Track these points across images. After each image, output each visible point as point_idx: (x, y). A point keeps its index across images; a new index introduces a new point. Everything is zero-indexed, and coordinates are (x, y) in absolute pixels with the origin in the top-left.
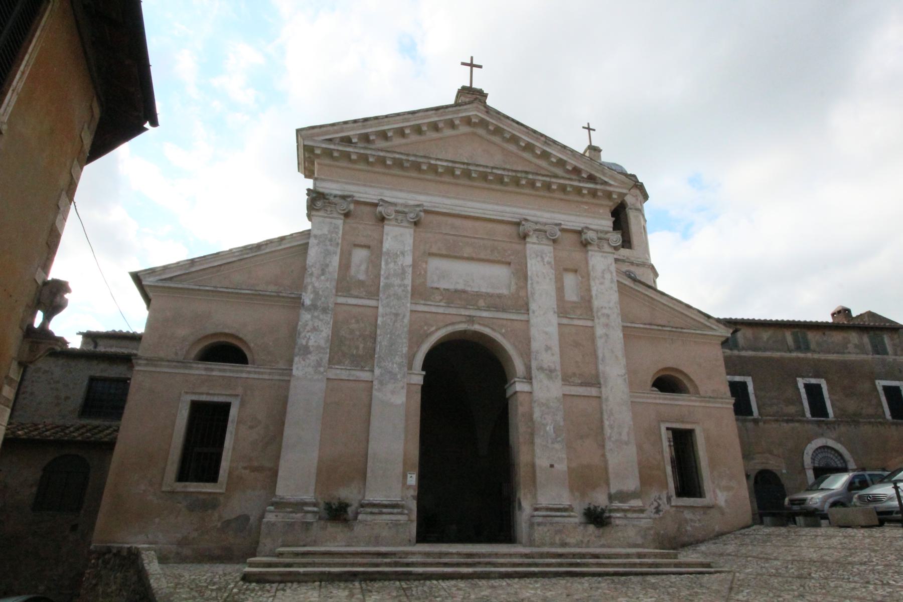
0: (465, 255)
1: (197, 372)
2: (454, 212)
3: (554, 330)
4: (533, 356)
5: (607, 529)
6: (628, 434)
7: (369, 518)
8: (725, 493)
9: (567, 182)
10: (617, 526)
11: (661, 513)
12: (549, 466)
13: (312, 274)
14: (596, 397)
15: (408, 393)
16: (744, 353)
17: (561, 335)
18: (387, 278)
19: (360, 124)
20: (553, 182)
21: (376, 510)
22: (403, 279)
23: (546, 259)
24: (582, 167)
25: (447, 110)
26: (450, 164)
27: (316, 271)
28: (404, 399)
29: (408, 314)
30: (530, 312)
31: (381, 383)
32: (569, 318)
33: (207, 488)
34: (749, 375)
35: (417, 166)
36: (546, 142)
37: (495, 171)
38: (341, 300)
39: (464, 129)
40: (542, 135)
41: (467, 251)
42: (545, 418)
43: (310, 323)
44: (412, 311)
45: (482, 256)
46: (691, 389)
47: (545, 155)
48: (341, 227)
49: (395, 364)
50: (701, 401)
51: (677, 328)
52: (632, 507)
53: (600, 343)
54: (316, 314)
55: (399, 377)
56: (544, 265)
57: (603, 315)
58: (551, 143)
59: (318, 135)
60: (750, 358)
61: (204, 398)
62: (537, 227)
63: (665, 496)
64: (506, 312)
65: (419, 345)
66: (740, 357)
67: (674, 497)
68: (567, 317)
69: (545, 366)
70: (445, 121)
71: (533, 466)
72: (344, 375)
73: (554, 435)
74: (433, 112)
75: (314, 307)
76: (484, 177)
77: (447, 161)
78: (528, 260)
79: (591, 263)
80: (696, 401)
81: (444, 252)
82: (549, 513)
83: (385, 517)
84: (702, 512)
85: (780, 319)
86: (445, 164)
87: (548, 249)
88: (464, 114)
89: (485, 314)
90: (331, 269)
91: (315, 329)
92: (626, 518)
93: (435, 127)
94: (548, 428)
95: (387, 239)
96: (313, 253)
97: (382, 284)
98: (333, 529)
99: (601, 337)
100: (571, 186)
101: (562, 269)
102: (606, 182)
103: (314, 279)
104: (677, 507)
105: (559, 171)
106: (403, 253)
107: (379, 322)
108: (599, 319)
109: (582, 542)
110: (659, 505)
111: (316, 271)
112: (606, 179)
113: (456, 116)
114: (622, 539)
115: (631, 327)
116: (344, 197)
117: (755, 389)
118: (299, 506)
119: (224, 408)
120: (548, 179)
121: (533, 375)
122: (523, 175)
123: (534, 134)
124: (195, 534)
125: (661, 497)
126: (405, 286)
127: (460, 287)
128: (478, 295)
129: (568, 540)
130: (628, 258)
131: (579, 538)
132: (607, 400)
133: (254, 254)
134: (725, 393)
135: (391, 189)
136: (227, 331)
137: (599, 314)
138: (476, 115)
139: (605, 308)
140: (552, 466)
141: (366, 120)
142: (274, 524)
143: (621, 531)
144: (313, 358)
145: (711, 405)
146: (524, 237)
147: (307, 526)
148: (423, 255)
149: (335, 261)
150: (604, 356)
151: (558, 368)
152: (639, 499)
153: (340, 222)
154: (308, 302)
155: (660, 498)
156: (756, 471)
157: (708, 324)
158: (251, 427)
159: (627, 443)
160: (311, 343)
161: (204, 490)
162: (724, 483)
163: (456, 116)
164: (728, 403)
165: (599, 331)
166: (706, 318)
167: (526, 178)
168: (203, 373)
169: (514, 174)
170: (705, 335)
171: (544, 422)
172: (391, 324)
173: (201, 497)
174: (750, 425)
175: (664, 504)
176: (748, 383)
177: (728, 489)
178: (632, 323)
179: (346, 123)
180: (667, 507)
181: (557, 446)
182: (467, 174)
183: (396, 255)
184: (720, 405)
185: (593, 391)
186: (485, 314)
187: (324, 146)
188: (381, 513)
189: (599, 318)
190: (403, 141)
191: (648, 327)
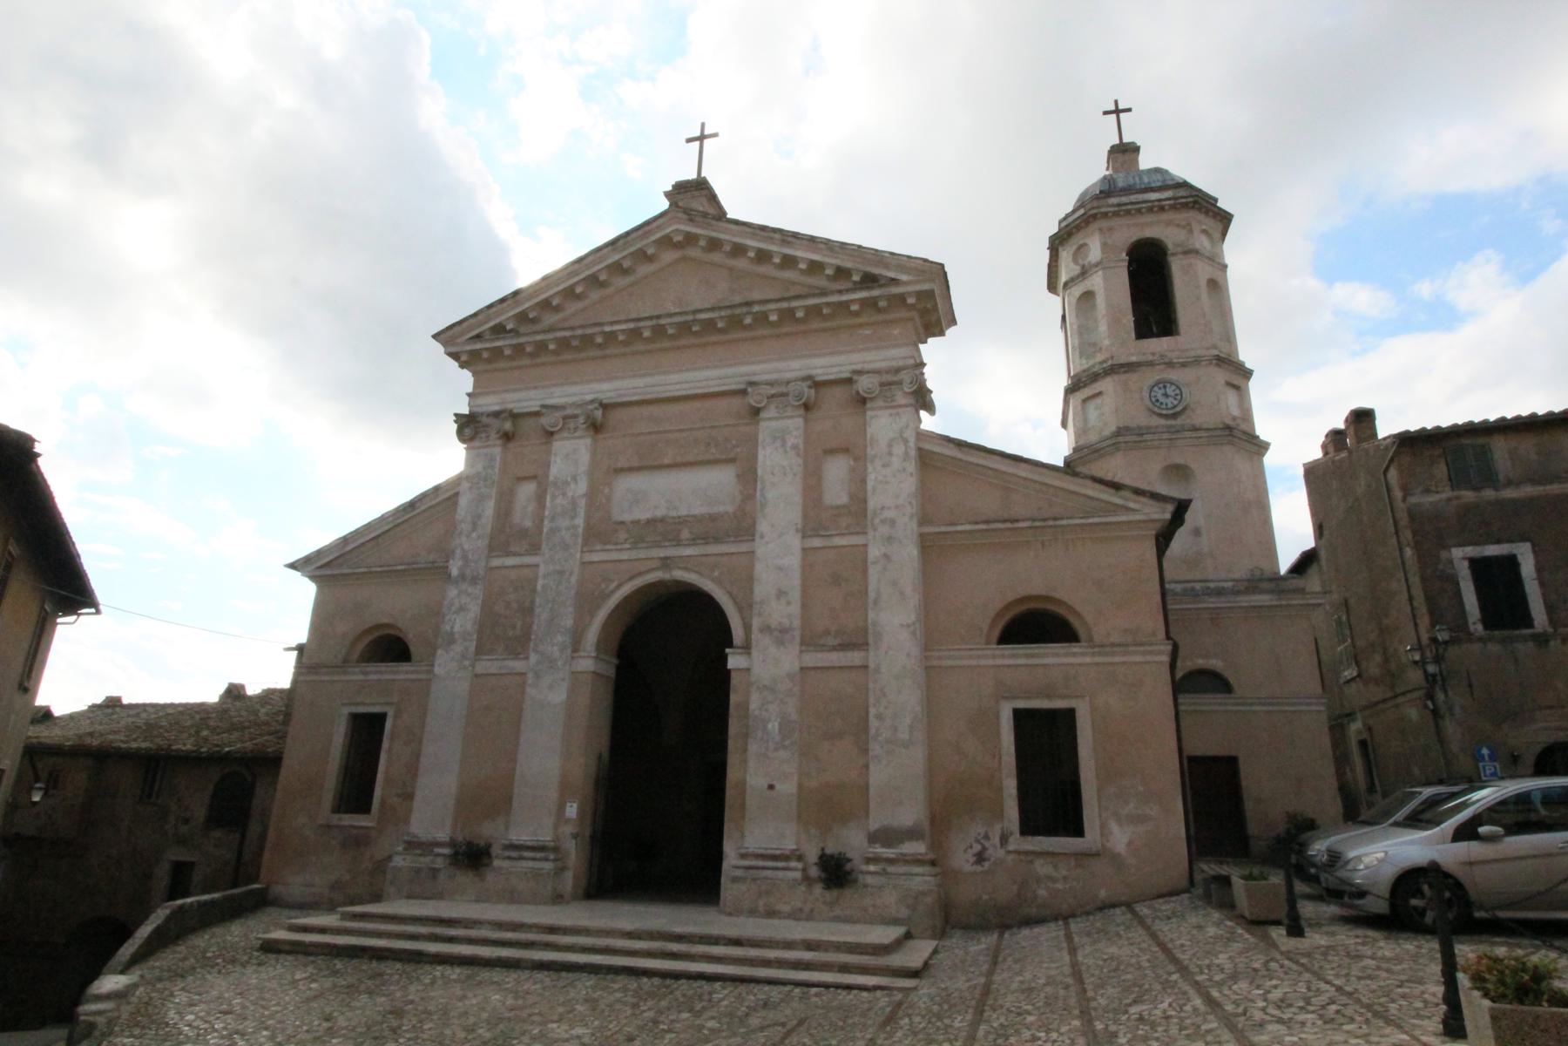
0: (666, 461)
1: (354, 677)
2: (649, 397)
3: (794, 561)
10: (866, 886)
11: (986, 864)
12: (766, 786)
13: (460, 534)
14: (861, 667)
15: (572, 690)
16: (1509, 493)
17: (807, 568)
18: (553, 519)
20: (795, 308)
21: (514, 854)
22: (573, 518)
23: (791, 441)
25: (629, 238)
26: (632, 325)
27: (465, 527)
28: (564, 696)
29: (576, 570)
30: (757, 536)
32: (823, 536)
33: (361, 821)
34: (1523, 539)
35: (587, 341)
36: (783, 241)
38: (496, 562)
39: (669, 256)
40: (775, 230)
42: (767, 710)
45: (691, 458)
47: (789, 262)
49: (555, 645)
50: (1094, 654)
51: (1045, 520)
52: (901, 854)
53: (873, 573)
55: (559, 663)
56: (786, 452)
57: (883, 521)
58: (790, 239)
59: (462, 334)
60: (1529, 503)
64: (723, 542)
65: (592, 614)
66: (1499, 503)
68: (818, 536)
72: (493, 667)
73: (778, 738)
74: (610, 248)
75: (462, 577)
76: (684, 328)
78: (760, 449)
80: (1083, 654)
81: (635, 464)
82: (760, 863)
83: (524, 864)
84: (1073, 863)
85: (1525, 412)
86: (624, 327)
87: (794, 425)
88: (658, 236)
89: (688, 551)
90: (483, 520)
92: (884, 873)
94: (770, 726)
95: (555, 462)
96: (463, 502)
97: (545, 530)
98: (464, 878)
99: (875, 563)
102: (893, 280)
103: (464, 539)
104: (1019, 853)
106: (574, 479)
108: (875, 530)
110: (984, 849)
111: (465, 527)
112: (891, 274)
114: (871, 909)
116: (496, 414)
117: (1539, 569)
118: (426, 847)
120: (785, 305)
121: (754, 643)
122: (744, 310)
123: (762, 233)
124: (348, 877)
125: (990, 834)
126: (575, 527)
127: (659, 513)
128: (682, 521)
132: (877, 670)
133: (408, 516)
134: (1154, 634)
137: (877, 521)
138: (677, 230)
139: (889, 508)
140: (771, 787)
143: (872, 895)
144: (458, 648)
145: (1116, 659)
146: (756, 412)
147: (434, 872)
148: (606, 472)
149: (489, 509)
150: (878, 593)
151: (797, 623)
152: (920, 842)
154: (455, 572)
155: (987, 837)
156: (1538, 749)
160: (457, 628)
161: (356, 824)
164: (1160, 653)
165: (874, 552)
166: (1112, 491)
168: (361, 677)
169: (729, 312)
172: (554, 587)
174: (1525, 649)
175: (995, 846)
176: (1520, 558)
179: (490, 306)
180: (1001, 853)
181: (782, 754)
182: (659, 331)
184: (1138, 658)
185: (855, 657)
186: (688, 551)
187: (468, 348)
188: (521, 858)
190: (579, 305)
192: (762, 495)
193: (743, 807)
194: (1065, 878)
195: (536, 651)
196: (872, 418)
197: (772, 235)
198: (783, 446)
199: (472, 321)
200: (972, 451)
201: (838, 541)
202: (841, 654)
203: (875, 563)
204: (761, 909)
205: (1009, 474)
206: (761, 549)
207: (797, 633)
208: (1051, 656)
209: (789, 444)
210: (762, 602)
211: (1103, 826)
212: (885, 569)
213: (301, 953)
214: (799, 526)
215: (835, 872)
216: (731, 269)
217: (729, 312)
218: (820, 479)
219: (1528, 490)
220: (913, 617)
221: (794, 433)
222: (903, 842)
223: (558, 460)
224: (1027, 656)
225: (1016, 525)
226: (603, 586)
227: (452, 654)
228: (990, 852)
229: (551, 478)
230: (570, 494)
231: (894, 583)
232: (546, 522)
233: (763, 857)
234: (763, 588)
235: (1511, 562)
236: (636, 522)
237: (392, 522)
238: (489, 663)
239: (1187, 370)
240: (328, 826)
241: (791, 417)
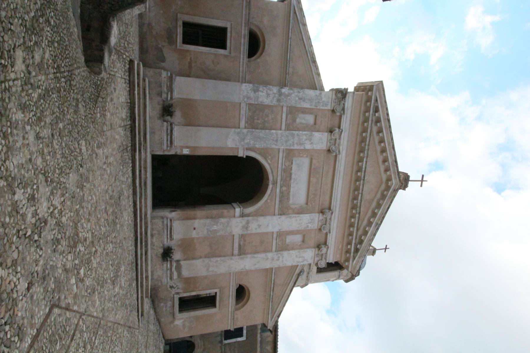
0: (311, 179)
2: (336, 171)
3: (270, 229)
4: (255, 218)
5: (161, 259)
7: (165, 128)
10: (163, 265)
11: (170, 289)
15: (232, 148)
16: (259, 335)
18: (298, 135)
19: (386, 117)
22: (297, 144)
23: (310, 225)
24: (363, 245)
25: (395, 167)
26: (363, 169)
28: (230, 146)
33: (180, 38)
34: (247, 338)
37: (360, 195)
38: (285, 109)
39: (384, 178)
40: (381, 222)
43: (271, 92)
45: (311, 188)
47: (370, 224)
49: (249, 140)
51: (272, 299)
53: (263, 255)
54: (277, 95)
55: (242, 143)
57: (279, 257)
60: (256, 340)
65: (260, 154)
66: (257, 333)
67: (179, 296)
69: (250, 225)
71: (194, 218)
73: (211, 229)
74: (394, 159)
75: (280, 94)
76: (357, 189)
77: (366, 168)
78: (309, 215)
81: (313, 167)
83: (165, 137)
84: (171, 312)
86: (364, 167)
87: (315, 226)
90: (302, 103)
91: (268, 95)
92: (167, 269)
94: (215, 226)
95: (320, 134)
96: (311, 93)
99: (266, 256)
101: (304, 234)
102: (355, 258)
106: (312, 143)
109: (154, 245)
110: (174, 288)
111: (301, 95)
116: (343, 109)
117: (239, 342)
118: (171, 89)
120: (356, 225)
121: (244, 218)
122: (358, 211)
126: (293, 145)
128: (289, 186)
131: (156, 244)
132: (231, 259)
137: (279, 255)
141: (389, 121)
142: (160, 76)
144: (252, 95)
147: (160, 94)
148: (311, 155)
149: (307, 105)
151: (249, 232)
153: (329, 107)
154: (283, 90)
155: (178, 288)
157: (274, 316)
158: (213, 62)
159: (208, 269)
160: (260, 93)
162: (187, 324)
164: (231, 327)
165: (270, 255)
169: (359, 206)
173: (175, 35)
174: (219, 339)
177: (184, 326)
179: (387, 109)
181: (206, 231)
182: (358, 179)
183: (310, 140)
187: (373, 97)
188: (167, 135)
192: (294, 217)
193: (188, 218)
194: (167, 310)
195: (248, 132)
196: (312, 251)
197: (380, 220)
198: (309, 223)
199: (383, 99)
200: (296, 278)
201: (274, 242)
202: (238, 247)
203: (266, 256)
204: (154, 232)
205: (287, 287)
206: (275, 218)
207: (245, 233)
208: (232, 300)
209: (309, 224)
210: (257, 220)
211: (182, 318)
212: (264, 259)
213: (130, 97)
214: (281, 230)
215: (167, 253)
216: (373, 200)
217: (359, 206)
218: (296, 234)
219: (259, 339)
220: (247, 269)
221: (312, 226)
222: (177, 272)
223: (320, 136)
224: (232, 295)
225: (272, 291)
226: (270, 157)
227: (250, 92)
228: (174, 290)
229: (314, 133)
230: (306, 142)
231: (258, 262)
232: (297, 132)
233: (171, 229)
234: (262, 220)
235: (241, 335)
236: (291, 169)
237: (309, 50)
238: (245, 109)
239: (306, 277)
240: (176, 20)
241: (318, 225)
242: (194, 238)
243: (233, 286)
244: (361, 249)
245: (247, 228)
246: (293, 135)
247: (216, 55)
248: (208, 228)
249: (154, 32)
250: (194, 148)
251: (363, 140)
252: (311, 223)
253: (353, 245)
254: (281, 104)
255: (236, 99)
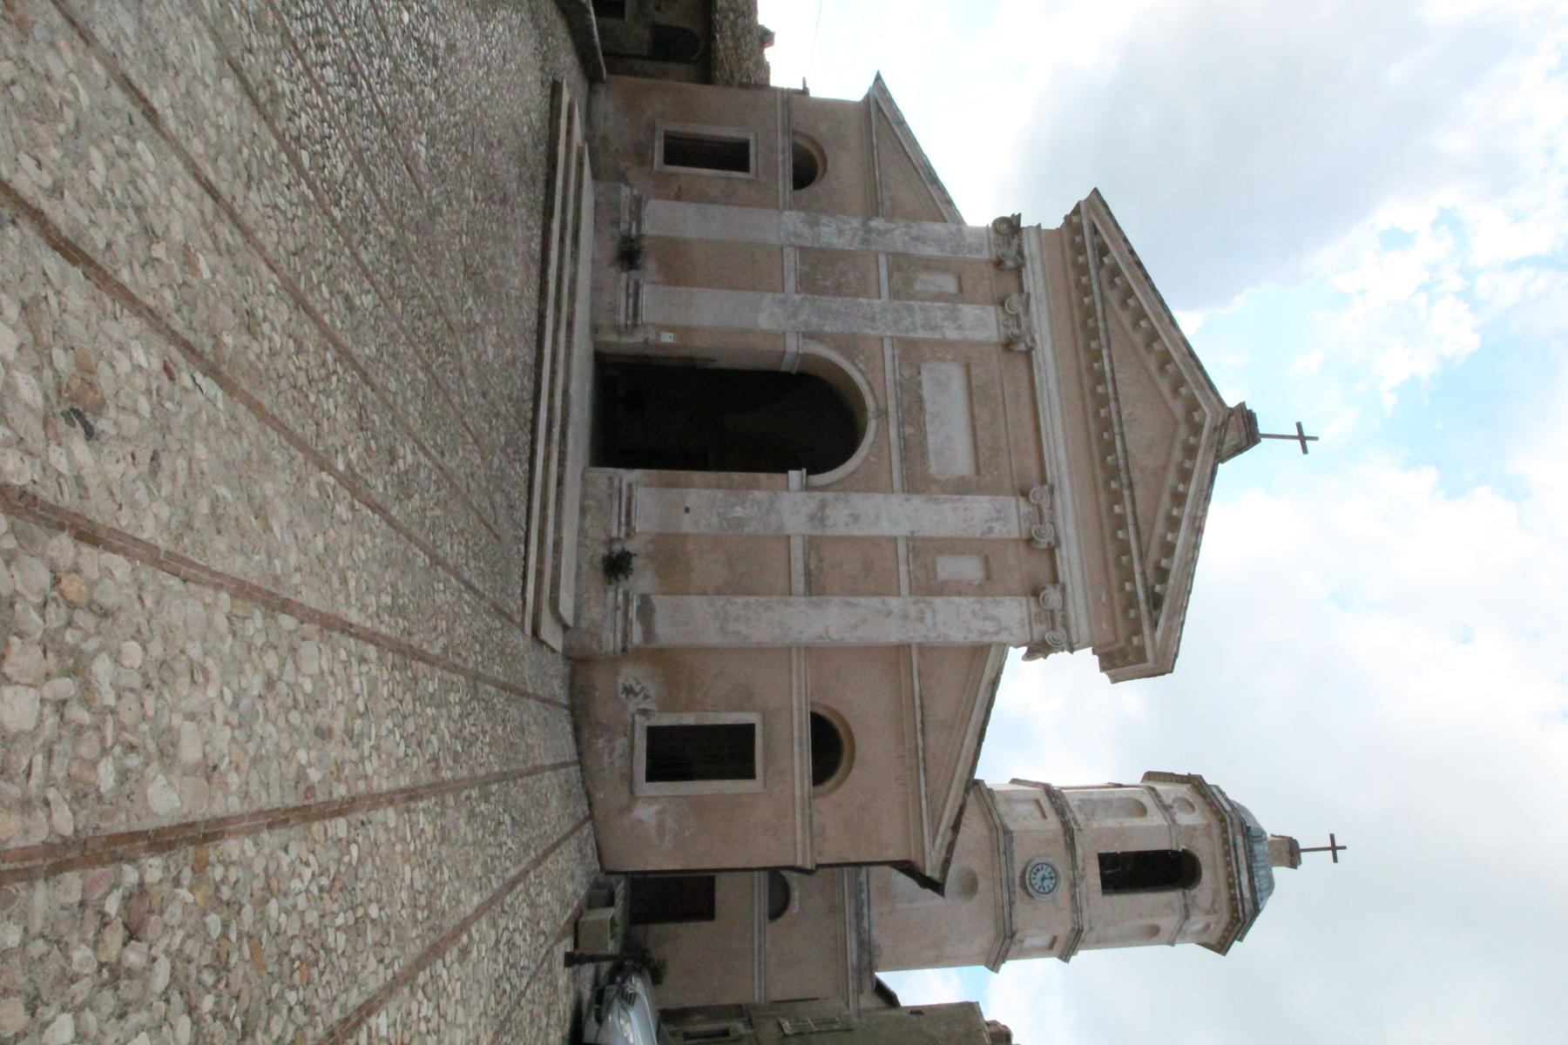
2: (1038, 391)
3: (885, 528)
4: (842, 495)
5: (600, 575)
6: (737, 633)
7: (623, 284)
8: (653, 822)
9: (1135, 552)
10: (605, 591)
11: (623, 696)
15: (768, 334)
19: (1131, 259)
22: (923, 327)
23: (997, 526)
24: (1171, 581)
25: (1196, 369)
26: (1108, 375)
27: (915, 230)
31: (783, 302)
35: (1093, 334)
37: (1118, 438)
38: (883, 260)
39: (1178, 409)
41: (984, 415)
43: (848, 227)
44: (881, 340)
45: (981, 434)
46: (820, 789)
47: (1173, 524)
48: (977, 257)
49: (808, 317)
50: (802, 798)
53: (875, 601)
54: (860, 232)
56: (986, 521)
57: (922, 611)
59: (1098, 215)
61: (752, 150)
62: (1045, 510)
63: (648, 707)
67: (649, 723)
69: (828, 511)
70: (1179, 374)
71: (687, 486)
75: (869, 230)
76: (1106, 425)
77: (1112, 370)
78: (989, 497)
79: (1007, 600)
81: (974, 383)
83: (623, 298)
84: (625, 771)
86: (1107, 368)
89: (893, 433)
90: (920, 246)
91: (840, 232)
92: (617, 608)
93: (1165, 359)
94: (739, 509)
96: (939, 228)
98: (611, 248)
99: (884, 603)
100: (1131, 561)
101: (984, 549)
104: (633, 725)
105: (1153, 554)
106: (960, 327)
107: (861, 300)
109: (586, 537)
110: (636, 695)
111: (915, 230)
112: (1162, 622)
113: (1192, 385)
115: (912, 674)
116: (1020, 253)
119: (744, 167)
120: (1130, 520)
122: (1125, 481)
127: (928, 406)
129: (589, 518)
130: (1082, 878)
131: (591, 532)
132: (787, 604)
134: (820, 853)
135: (1050, 312)
136: (829, 164)
137: (923, 606)
139: (934, 616)
140: (687, 510)
141: (1139, 264)
142: (618, 194)
144: (806, 230)
147: (616, 223)
148: (965, 355)
149: (932, 251)
151: (829, 532)
153: (986, 255)
154: (874, 223)
155: (646, 697)
157: (942, 830)
158: (723, 191)
159: (723, 630)
160: (824, 229)
162: (670, 823)
163: (1192, 385)
164: (804, 858)
165: (894, 603)
166: (951, 824)
167: (1121, 485)
168: (780, 147)
170: (921, 821)
171: (748, 504)
173: (650, 152)
177: (661, 826)
178: (920, 675)
179: (1126, 240)
180: (632, 708)
183: (955, 320)
185: (799, 582)
186: (893, 433)
187: (1085, 223)
188: (628, 296)
189: (915, 603)
191: (917, 702)
194: (612, 764)
198: (992, 520)
201: (903, 569)
207: (819, 532)
208: (801, 759)
209: (994, 524)
221: (1004, 530)
225: (919, 734)
233: (630, 499)
234: (859, 501)
236: (919, 385)
242: (686, 536)
243: (800, 709)
244: (1169, 592)
245: (822, 520)
246: (910, 310)
247: (729, 179)
248: (721, 510)
249: (613, 149)
250: (683, 331)
251: (1089, 312)
252: (997, 519)
253: (1138, 577)
254: (873, 248)
255: (773, 238)
